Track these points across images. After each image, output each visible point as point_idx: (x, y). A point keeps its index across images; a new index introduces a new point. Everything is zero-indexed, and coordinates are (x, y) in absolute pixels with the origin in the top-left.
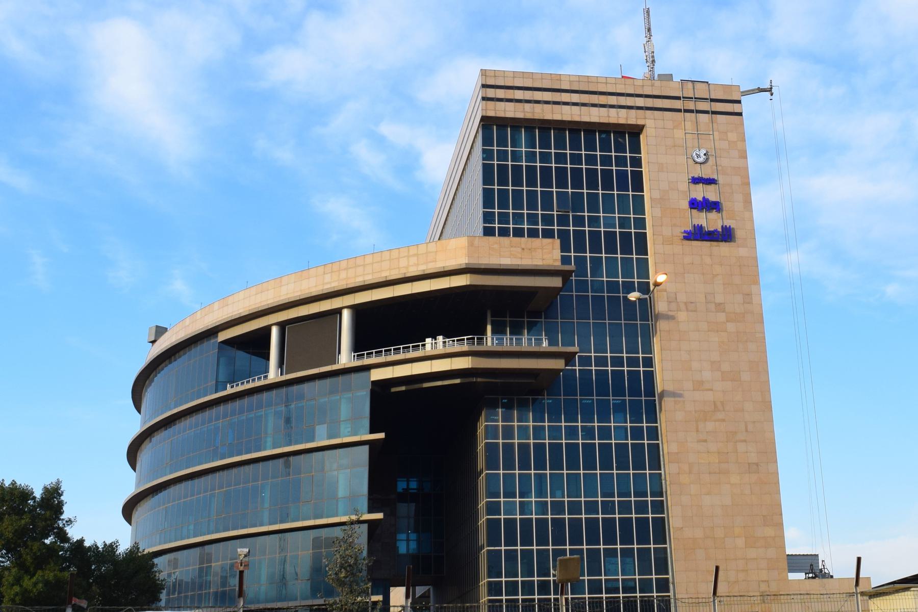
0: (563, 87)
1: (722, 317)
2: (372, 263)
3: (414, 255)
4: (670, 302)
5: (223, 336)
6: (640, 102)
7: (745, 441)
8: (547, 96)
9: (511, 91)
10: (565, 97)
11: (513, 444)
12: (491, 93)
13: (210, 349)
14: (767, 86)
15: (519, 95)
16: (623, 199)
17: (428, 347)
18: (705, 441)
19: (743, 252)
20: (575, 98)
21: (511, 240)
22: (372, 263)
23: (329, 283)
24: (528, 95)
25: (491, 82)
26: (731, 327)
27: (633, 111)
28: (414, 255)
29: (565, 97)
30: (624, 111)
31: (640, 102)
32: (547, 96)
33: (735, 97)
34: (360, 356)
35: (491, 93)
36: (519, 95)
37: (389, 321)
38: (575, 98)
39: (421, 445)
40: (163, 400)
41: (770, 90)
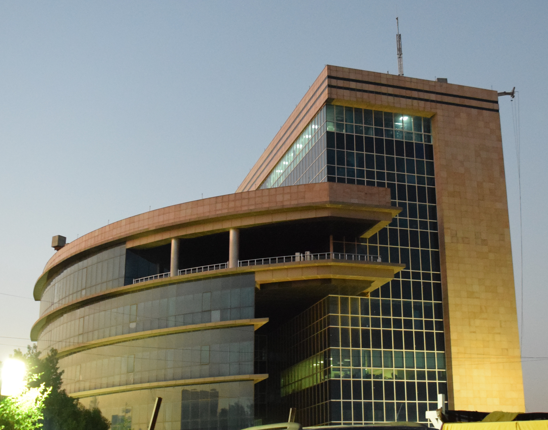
0: (488, 112)
1: (485, 249)
2: (255, 198)
3: (288, 193)
4: (452, 237)
5: (130, 245)
6: (433, 97)
7: (499, 334)
8: (372, 88)
9: (348, 82)
10: (384, 89)
11: (348, 329)
12: (334, 82)
13: (121, 251)
14: (510, 91)
15: (353, 85)
16: (420, 164)
17: (297, 259)
18: (475, 332)
19: (499, 205)
20: (390, 90)
21: (355, 187)
22: (255, 198)
23: (221, 210)
24: (359, 86)
25: (334, 74)
26: (492, 256)
27: (428, 103)
28: (288, 193)
29: (384, 89)
30: (423, 102)
31: (433, 97)
32: (372, 88)
33: (493, 99)
34: (245, 264)
35: (334, 82)
36: (353, 85)
37: (267, 240)
38: (390, 90)
39: (287, 327)
40: (59, 292)
41: (512, 94)
